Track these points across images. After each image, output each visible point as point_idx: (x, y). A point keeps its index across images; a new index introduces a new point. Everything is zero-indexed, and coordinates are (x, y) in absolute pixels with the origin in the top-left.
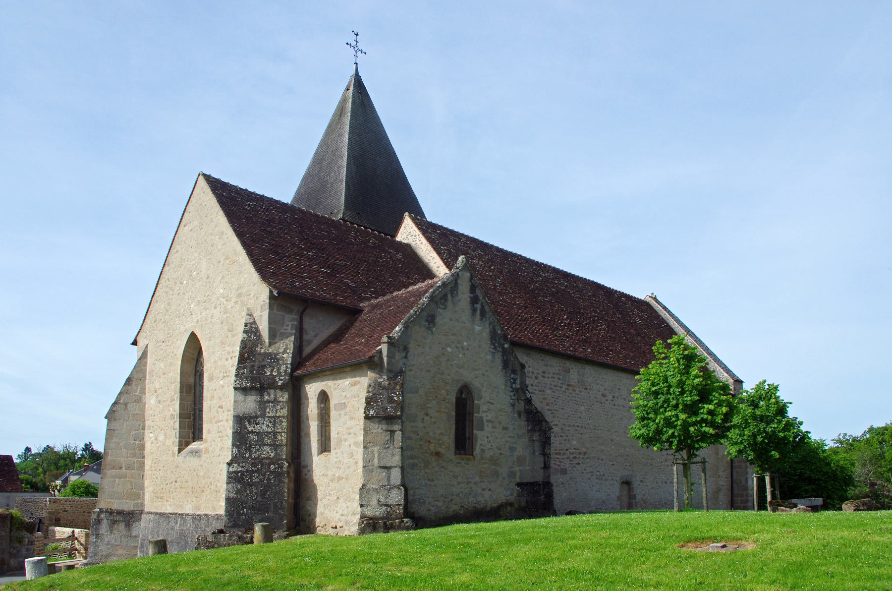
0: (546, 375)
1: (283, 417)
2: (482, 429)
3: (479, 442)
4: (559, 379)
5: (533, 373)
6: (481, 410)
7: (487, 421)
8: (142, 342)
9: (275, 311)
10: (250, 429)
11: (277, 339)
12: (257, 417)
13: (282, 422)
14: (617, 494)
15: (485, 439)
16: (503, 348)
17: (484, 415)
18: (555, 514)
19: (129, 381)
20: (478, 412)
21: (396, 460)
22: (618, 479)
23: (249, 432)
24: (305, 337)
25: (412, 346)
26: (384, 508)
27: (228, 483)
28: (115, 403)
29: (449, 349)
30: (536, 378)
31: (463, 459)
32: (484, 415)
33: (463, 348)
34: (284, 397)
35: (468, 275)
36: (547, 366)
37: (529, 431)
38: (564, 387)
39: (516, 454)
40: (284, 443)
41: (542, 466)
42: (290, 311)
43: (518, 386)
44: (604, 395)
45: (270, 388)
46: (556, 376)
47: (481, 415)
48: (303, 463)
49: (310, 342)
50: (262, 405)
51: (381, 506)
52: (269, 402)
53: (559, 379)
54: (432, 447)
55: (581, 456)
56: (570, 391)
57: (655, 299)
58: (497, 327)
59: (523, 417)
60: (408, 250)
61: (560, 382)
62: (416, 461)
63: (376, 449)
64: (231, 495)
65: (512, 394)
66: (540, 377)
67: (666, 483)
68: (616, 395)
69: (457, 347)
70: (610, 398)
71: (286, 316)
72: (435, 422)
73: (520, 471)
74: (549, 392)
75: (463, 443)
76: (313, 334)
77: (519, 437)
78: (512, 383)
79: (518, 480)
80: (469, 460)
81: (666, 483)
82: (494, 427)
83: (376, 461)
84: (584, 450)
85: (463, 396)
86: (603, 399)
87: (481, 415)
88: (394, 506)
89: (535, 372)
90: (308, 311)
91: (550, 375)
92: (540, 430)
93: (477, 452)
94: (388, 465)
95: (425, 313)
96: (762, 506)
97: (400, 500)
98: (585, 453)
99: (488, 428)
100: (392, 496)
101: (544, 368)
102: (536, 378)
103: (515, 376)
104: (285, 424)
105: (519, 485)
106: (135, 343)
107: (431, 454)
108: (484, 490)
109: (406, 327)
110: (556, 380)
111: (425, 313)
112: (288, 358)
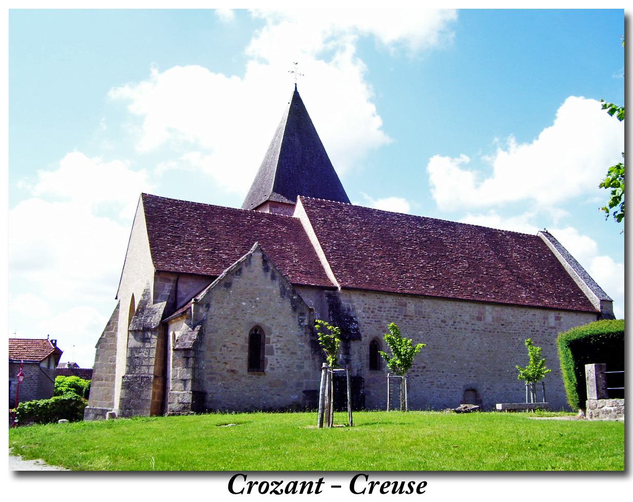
0: (383, 310)
1: (154, 348)
2: (272, 354)
3: (269, 363)
4: (395, 311)
5: (369, 308)
6: (271, 341)
7: (276, 349)
9: (158, 282)
10: (136, 356)
11: (159, 300)
12: (140, 348)
15: (273, 361)
17: (274, 345)
18: (210, 411)
19: (109, 324)
20: (269, 343)
21: (189, 376)
22: (461, 387)
23: (135, 358)
25: (213, 303)
27: (122, 389)
28: (101, 338)
29: (244, 304)
30: (372, 312)
31: (254, 375)
32: (274, 345)
33: (256, 302)
35: (260, 254)
36: (383, 302)
39: (303, 371)
42: (169, 281)
43: (306, 324)
44: (443, 321)
46: (392, 310)
47: (271, 344)
48: (167, 377)
49: (182, 299)
53: (395, 311)
54: (228, 367)
55: (421, 370)
57: (548, 234)
58: (286, 286)
60: (297, 224)
61: (397, 314)
62: (214, 376)
63: (178, 368)
64: (123, 397)
65: (300, 330)
67: (518, 390)
69: (250, 302)
71: (166, 284)
72: (231, 351)
73: (306, 382)
77: (306, 358)
79: (304, 389)
80: (260, 375)
81: (518, 390)
82: (283, 352)
83: (178, 376)
84: (423, 365)
85: (258, 333)
86: (443, 325)
87: (271, 344)
89: (371, 307)
91: (386, 310)
93: (267, 369)
94: (185, 378)
95: (223, 282)
96: (404, 409)
98: (424, 367)
99: (277, 354)
101: (381, 305)
102: (372, 312)
105: (304, 392)
106: (116, 298)
107: (228, 371)
108: (273, 395)
109: (209, 292)
110: (393, 312)
111: (223, 282)
112: (161, 311)
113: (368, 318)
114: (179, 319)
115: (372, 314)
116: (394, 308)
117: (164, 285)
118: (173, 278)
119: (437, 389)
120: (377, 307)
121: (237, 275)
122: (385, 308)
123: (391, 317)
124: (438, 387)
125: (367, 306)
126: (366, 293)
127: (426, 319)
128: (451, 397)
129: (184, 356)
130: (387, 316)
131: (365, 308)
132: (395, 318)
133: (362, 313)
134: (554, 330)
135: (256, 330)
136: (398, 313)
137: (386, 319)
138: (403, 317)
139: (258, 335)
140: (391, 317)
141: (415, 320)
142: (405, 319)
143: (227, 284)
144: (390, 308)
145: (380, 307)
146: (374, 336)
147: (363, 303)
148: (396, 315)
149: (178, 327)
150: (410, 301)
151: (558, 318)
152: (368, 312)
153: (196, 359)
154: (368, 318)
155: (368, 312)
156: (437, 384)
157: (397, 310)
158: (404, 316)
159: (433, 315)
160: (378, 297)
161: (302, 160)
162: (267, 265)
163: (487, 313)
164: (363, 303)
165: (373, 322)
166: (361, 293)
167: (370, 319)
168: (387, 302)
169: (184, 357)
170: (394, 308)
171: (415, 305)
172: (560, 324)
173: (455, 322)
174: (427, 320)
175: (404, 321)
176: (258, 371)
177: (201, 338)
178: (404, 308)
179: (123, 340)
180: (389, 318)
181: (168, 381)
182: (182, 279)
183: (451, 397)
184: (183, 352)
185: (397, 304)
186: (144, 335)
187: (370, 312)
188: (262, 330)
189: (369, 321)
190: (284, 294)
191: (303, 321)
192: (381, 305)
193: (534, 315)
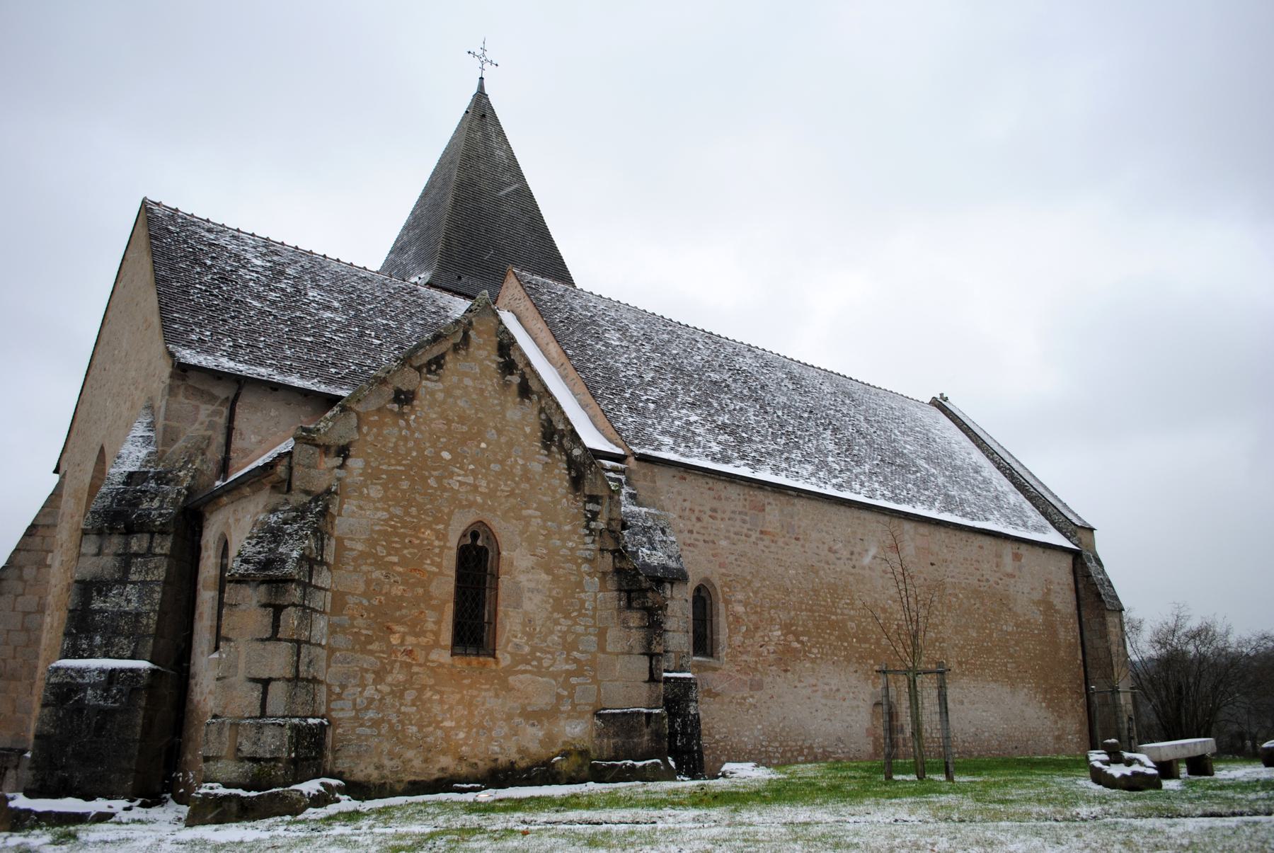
0: (719, 515)
4: (744, 522)
5: (692, 510)
8: (62, 471)
13: (153, 591)
14: (867, 724)
16: (569, 456)
19: (32, 530)
24: (237, 443)
26: (248, 765)
30: (699, 519)
34: (164, 546)
36: (719, 498)
37: (620, 610)
38: (755, 535)
40: (151, 631)
41: (647, 677)
42: (212, 398)
43: (602, 526)
45: (141, 532)
46: (738, 517)
48: (192, 670)
49: (247, 454)
50: (126, 559)
51: (242, 760)
52: (136, 555)
56: (767, 543)
59: (611, 583)
66: (706, 518)
67: (962, 703)
68: (856, 550)
70: (845, 554)
71: (203, 407)
74: (724, 543)
75: (473, 630)
76: (254, 439)
78: (589, 520)
85: (479, 543)
86: (831, 556)
88: (267, 760)
89: (697, 508)
90: (244, 392)
91: (726, 516)
92: (645, 608)
97: (278, 749)
100: (263, 738)
101: (716, 504)
102: (699, 519)
103: (596, 508)
104: (157, 596)
106: (56, 471)
110: (738, 523)
113: (691, 532)
114: (247, 490)
115: (699, 524)
116: (740, 513)
117: (197, 408)
118: (222, 392)
119: (824, 701)
120: (707, 509)
121: (430, 372)
122: (724, 512)
123: (736, 534)
124: (826, 697)
125: (687, 504)
126: (685, 475)
127: (802, 542)
128: (849, 719)
129: (264, 601)
130: (728, 531)
131: (683, 510)
132: (743, 538)
133: (678, 520)
134: (1012, 581)
135: (475, 536)
136: (748, 526)
137: (727, 538)
138: (758, 535)
139: (482, 548)
140: (736, 534)
141: (780, 544)
142: (762, 540)
143: (403, 392)
144: (733, 512)
145: (714, 510)
146: (702, 576)
147: (680, 498)
148: (745, 531)
149: (238, 520)
150: (771, 500)
151: (1017, 557)
152: (689, 519)
153: (304, 611)
154: (691, 532)
155: (689, 519)
156: (824, 691)
157: (747, 518)
158: (762, 532)
159: (814, 535)
160: (711, 485)
161: (481, 218)
162: (509, 356)
163: (906, 537)
164: (680, 498)
165: (701, 544)
166: (676, 473)
167: (695, 535)
168: (727, 499)
169: (265, 606)
170: (740, 513)
171: (782, 511)
172: (1020, 568)
173: (852, 553)
174: (803, 546)
175: (761, 545)
176: (478, 655)
177: (322, 550)
178: (761, 515)
179: (65, 534)
180: (732, 535)
181: (192, 682)
182: (247, 398)
183: (849, 719)
184: (263, 588)
185: (747, 503)
186: (127, 545)
187: (694, 519)
188: (491, 536)
189: (692, 541)
190: (551, 439)
191: (595, 515)
192: (716, 504)
193: (981, 547)
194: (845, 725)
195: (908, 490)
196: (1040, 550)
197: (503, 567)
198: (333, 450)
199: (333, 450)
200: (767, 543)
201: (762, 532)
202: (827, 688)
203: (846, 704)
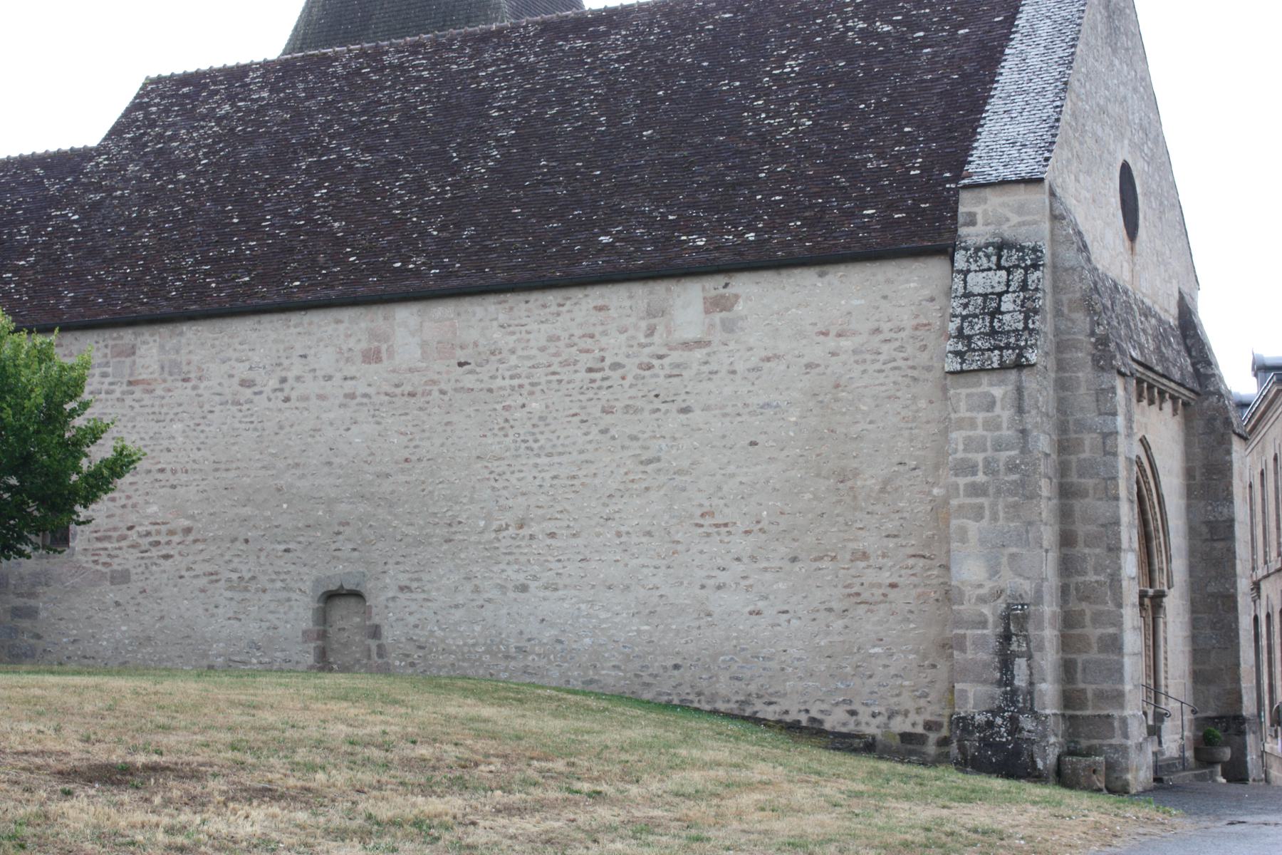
4: (104, 375)
68: (291, 375)
119: (229, 594)
124: (231, 588)
148: (105, 387)
156: (229, 580)
157: (110, 370)
171: (162, 347)
173: (284, 380)
175: (129, 401)
178: (128, 361)
185: (108, 351)
194: (265, 625)
195: (177, 270)
196: (1022, 186)
197: (1205, 822)
198: (1062, 394)
199: (1062, 394)
200: (137, 395)
201: (130, 383)
202: (234, 576)
203: (267, 597)
